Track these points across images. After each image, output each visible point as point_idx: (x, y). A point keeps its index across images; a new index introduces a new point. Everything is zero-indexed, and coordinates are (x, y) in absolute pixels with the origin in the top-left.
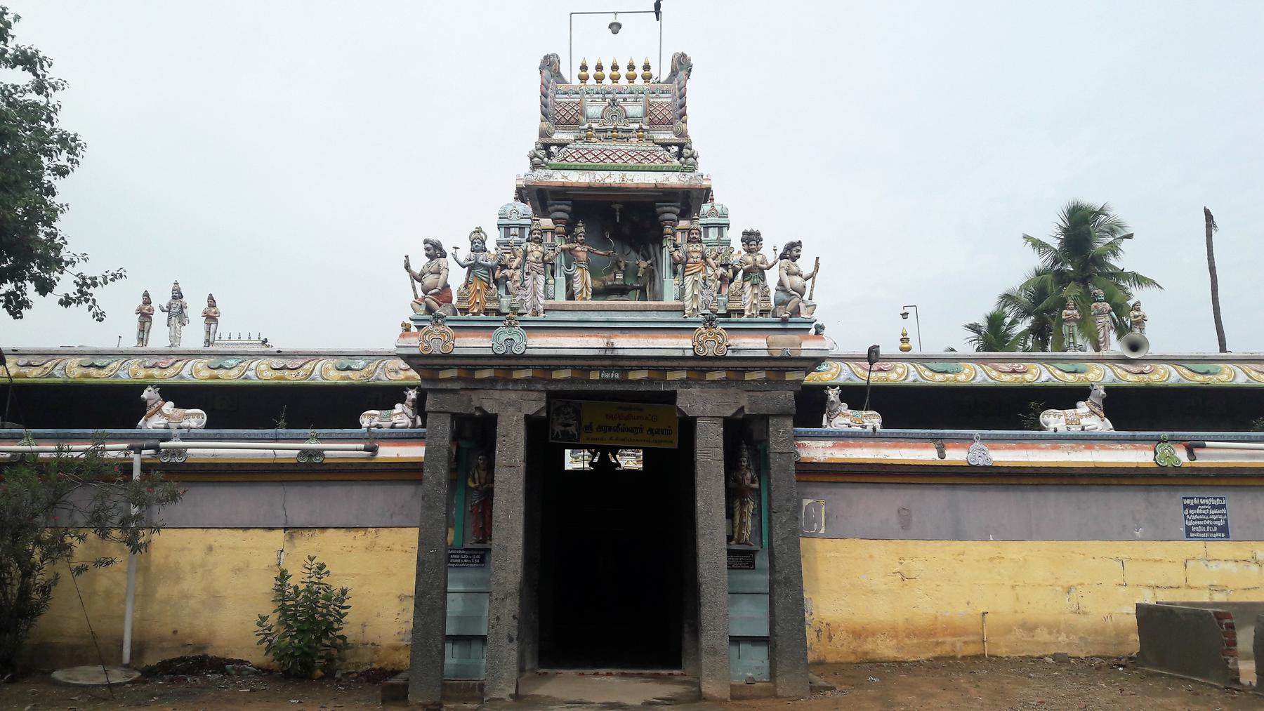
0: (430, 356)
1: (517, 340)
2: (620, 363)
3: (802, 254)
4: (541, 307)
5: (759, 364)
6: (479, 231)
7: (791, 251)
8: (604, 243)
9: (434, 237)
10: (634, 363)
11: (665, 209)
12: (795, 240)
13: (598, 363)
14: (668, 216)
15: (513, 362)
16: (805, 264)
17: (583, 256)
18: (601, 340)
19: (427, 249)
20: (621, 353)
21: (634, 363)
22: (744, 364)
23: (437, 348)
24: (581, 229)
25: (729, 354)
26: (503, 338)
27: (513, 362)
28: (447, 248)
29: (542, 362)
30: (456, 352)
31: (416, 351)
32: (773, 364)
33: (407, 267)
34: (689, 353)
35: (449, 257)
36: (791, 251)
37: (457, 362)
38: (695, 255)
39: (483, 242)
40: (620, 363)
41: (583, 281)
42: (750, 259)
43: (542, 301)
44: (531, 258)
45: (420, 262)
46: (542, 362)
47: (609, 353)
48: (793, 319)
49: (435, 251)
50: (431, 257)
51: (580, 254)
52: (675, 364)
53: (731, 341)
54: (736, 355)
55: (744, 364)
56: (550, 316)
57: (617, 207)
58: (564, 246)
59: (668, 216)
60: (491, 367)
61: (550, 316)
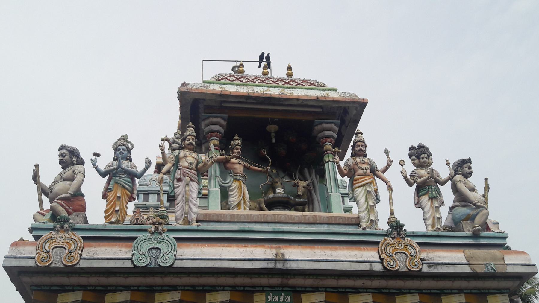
0: (49, 271)
1: (164, 249)
2: (293, 281)
3: (473, 170)
4: (194, 216)
5: (458, 284)
6: (124, 138)
7: (463, 167)
8: (261, 160)
9: (70, 144)
10: (309, 282)
11: (325, 125)
12: (466, 157)
13: (264, 281)
14: (327, 133)
15: (158, 280)
16: (476, 180)
17: (240, 168)
18: (268, 251)
19: (62, 155)
20: (294, 266)
21: (309, 282)
22: (441, 284)
23: (58, 259)
24: (237, 142)
25: (425, 269)
26: (145, 247)
27: (158, 280)
28: (86, 155)
29: (193, 280)
30: (83, 264)
31: (31, 263)
32: (474, 284)
33: (36, 178)
34: (378, 267)
35: (88, 166)
36: (463, 167)
37: (83, 280)
38: (364, 166)
39: (129, 151)
40: (293, 281)
41: (239, 192)
42: (423, 172)
43: (195, 209)
44: (184, 163)
45: (51, 172)
46: (193, 280)
47: (280, 266)
48: (483, 234)
49: (70, 158)
50: (64, 164)
51: (237, 166)
52: (359, 283)
53: (423, 255)
54: (433, 270)
55: (441, 284)
56: (204, 226)
57: (272, 128)
58: (219, 157)
59: (327, 133)
60: (127, 288)
61: (204, 226)
